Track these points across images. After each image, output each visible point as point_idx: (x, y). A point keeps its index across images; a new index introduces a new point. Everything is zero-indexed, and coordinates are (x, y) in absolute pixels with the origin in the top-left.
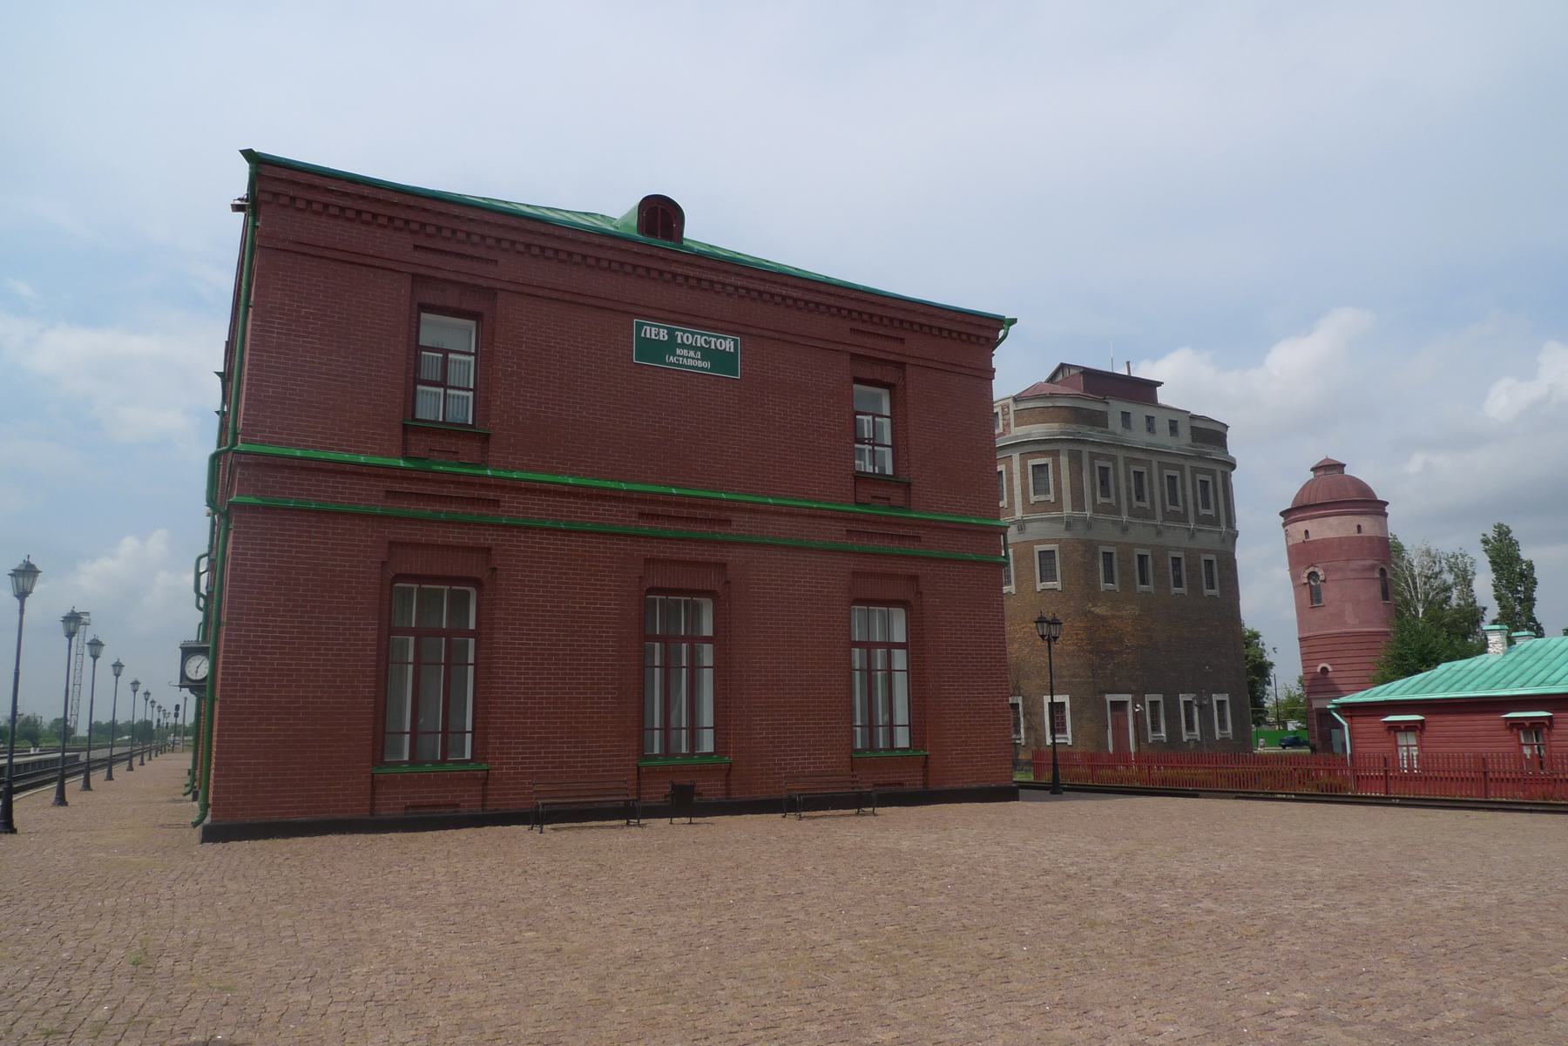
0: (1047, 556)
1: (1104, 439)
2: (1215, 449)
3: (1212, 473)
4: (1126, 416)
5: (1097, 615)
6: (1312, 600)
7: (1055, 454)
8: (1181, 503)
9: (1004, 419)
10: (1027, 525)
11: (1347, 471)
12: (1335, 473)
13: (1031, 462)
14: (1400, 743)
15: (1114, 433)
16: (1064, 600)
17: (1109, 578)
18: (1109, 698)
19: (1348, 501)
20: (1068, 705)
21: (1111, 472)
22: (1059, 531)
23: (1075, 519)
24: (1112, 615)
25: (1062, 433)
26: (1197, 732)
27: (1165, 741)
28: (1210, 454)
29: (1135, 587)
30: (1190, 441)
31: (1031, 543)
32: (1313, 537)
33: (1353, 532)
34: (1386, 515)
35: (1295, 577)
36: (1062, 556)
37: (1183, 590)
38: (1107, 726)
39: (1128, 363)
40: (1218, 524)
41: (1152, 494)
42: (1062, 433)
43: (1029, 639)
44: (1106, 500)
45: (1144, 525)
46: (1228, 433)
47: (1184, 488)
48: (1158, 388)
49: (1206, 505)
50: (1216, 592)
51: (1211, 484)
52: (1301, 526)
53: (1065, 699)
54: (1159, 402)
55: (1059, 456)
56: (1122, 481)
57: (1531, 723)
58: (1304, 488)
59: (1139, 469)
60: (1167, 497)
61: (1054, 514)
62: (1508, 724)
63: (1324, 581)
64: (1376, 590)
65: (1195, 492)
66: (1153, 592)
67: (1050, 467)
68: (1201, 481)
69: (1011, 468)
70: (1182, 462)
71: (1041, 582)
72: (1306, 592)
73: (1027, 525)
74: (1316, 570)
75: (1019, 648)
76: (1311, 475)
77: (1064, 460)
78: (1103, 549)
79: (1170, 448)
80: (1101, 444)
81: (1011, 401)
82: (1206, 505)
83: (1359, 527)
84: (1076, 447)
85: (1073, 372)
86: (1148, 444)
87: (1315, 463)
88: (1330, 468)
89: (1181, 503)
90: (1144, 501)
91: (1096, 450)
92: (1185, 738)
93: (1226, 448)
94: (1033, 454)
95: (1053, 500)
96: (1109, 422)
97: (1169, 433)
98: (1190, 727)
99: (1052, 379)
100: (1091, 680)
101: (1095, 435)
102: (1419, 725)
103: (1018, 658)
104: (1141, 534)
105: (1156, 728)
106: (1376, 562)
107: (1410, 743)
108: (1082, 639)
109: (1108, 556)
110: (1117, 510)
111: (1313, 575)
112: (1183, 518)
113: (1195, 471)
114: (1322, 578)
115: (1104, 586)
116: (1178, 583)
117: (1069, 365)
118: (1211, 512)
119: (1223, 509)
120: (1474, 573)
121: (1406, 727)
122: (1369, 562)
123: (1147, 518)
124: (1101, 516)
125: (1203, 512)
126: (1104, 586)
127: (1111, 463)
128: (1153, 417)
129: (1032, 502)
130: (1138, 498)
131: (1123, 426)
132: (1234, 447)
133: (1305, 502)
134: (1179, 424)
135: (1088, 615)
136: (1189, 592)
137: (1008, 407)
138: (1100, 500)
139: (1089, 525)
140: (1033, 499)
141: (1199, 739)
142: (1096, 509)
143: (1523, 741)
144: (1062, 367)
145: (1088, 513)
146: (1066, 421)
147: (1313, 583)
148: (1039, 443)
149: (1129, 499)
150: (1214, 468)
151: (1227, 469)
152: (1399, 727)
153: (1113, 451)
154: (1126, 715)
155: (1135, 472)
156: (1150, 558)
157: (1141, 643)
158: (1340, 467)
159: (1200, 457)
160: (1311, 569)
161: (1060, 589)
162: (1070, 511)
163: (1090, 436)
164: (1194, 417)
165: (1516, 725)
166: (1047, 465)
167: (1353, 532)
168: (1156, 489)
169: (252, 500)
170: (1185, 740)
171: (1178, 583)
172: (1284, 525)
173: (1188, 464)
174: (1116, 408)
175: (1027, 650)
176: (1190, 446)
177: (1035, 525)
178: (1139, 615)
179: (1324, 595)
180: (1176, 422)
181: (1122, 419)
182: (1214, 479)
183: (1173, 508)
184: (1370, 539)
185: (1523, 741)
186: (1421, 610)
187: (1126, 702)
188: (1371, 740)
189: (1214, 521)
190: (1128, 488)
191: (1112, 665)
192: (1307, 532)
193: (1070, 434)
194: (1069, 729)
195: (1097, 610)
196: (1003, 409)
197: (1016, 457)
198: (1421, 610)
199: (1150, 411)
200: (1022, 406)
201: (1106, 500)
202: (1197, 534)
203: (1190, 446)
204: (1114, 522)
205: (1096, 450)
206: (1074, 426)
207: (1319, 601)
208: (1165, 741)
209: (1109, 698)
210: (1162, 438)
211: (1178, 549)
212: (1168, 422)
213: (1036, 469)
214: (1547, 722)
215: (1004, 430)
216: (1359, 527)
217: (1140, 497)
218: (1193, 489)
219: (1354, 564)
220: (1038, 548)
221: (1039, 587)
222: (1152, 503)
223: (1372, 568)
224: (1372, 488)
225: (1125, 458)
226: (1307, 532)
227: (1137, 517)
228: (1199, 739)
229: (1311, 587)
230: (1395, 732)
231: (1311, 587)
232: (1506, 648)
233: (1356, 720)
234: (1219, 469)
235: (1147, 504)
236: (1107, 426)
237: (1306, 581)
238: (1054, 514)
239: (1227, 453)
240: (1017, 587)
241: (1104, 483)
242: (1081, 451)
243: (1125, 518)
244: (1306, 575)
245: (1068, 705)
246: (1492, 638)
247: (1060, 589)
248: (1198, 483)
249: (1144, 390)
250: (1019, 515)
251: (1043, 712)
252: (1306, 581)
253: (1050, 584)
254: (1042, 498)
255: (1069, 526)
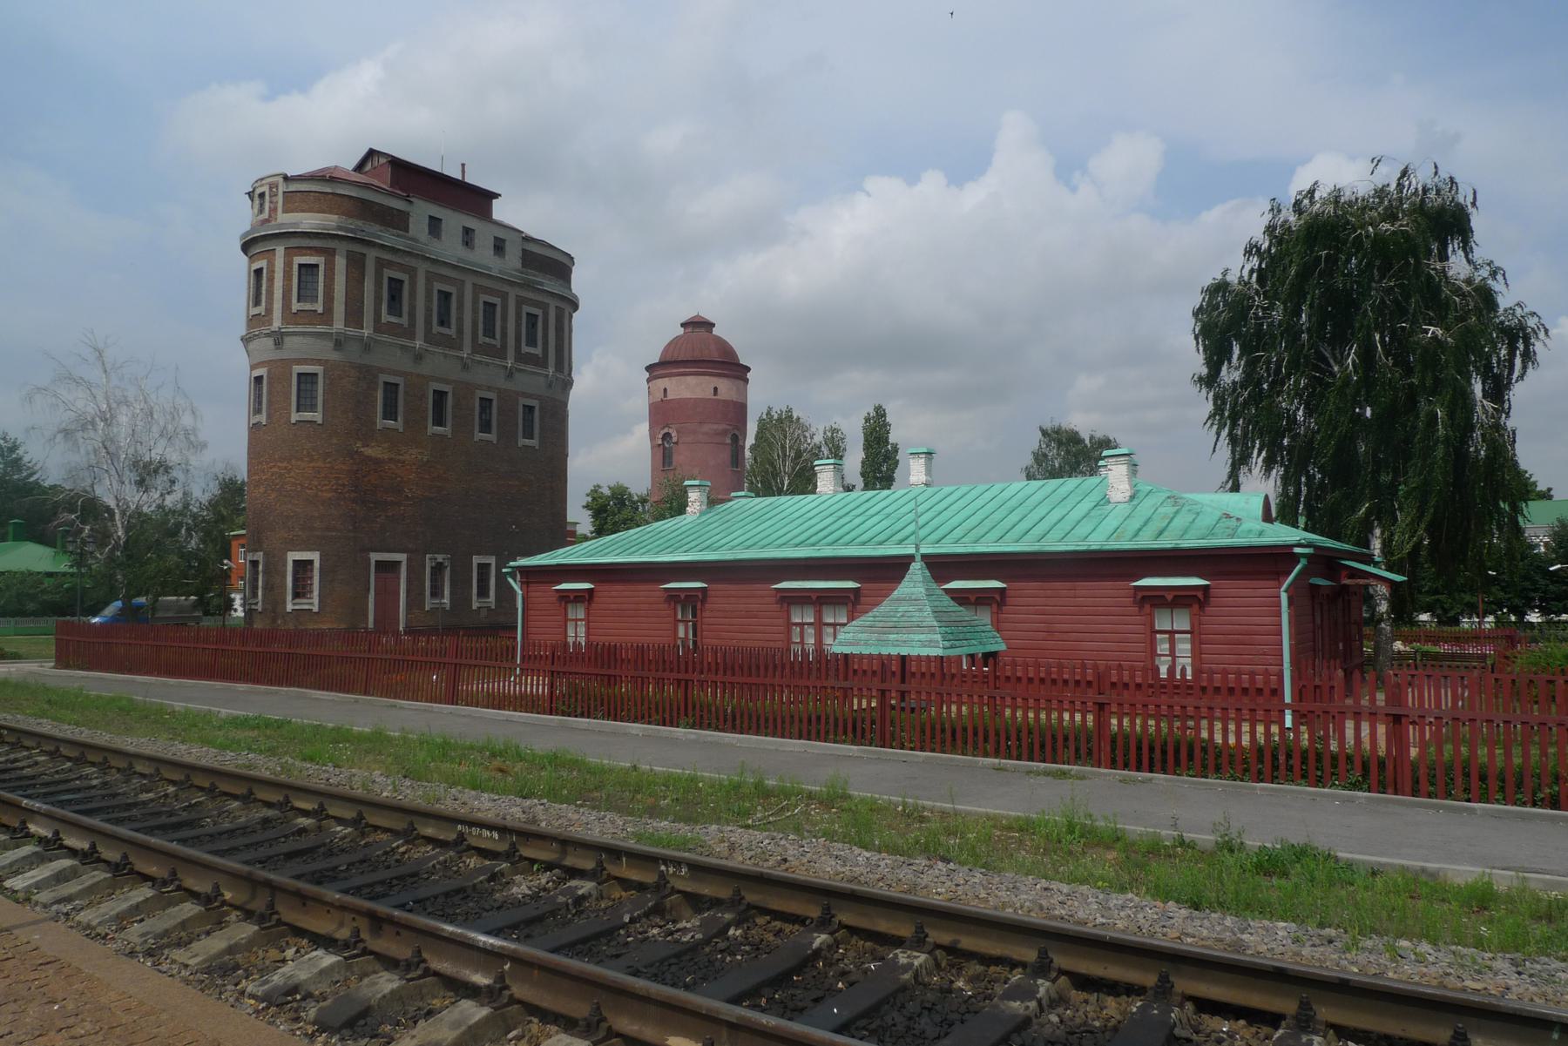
0: (306, 379)
1: (399, 243)
2: (550, 280)
3: (544, 307)
4: (435, 224)
5: (369, 458)
6: (664, 463)
7: (329, 253)
8: (498, 336)
9: (271, 202)
10: (287, 339)
11: (715, 331)
12: (702, 333)
13: (299, 260)
14: (570, 616)
15: (415, 240)
16: (324, 436)
17: (390, 413)
18: (375, 557)
19: (709, 361)
20: (317, 564)
21: (406, 287)
22: (326, 351)
23: (348, 338)
24: (390, 459)
25: (340, 228)
26: (446, 600)
27: (448, 608)
28: (542, 284)
29: (426, 428)
30: (518, 265)
31: (287, 363)
32: (670, 397)
33: (709, 394)
34: (747, 381)
35: (652, 437)
36: (327, 382)
37: (492, 437)
38: (369, 589)
39: (463, 165)
40: (544, 365)
41: (460, 320)
42: (340, 228)
43: (277, 481)
44: (393, 319)
45: (446, 356)
46: (574, 268)
47: (504, 319)
48: (494, 201)
49: (532, 342)
50: (534, 442)
51: (499, 309)
52: (662, 383)
53: (315, 556)
54: (494, 217)
55: (334, 255)
56: (420, 300)
57: (1175, 596)
58: (669, 344)
59: (446, 288)
60: (481, 326)
61: (320, 329)
62: (1139, 597)
63: (676, 443)
64: (725, 455)
65: (518, 325)
66: (450, 436)
67: (322, 268)
68: (528, 314)
69: (273, 265)
70: (506, 288)
71: (298, 411)
72: (660, 452)
73: (287, 339)
74: (671, 431)
75: (265, 492)
76: (681, 331)
77: (340, 263)
78: (383, 378)
79: (489, 269)
80: (393, 250)
81: (281, 180)
82: (532, 342)
83: (716, 389)
84: (357, 248)
85: (383, 160)
86: (460, 260)
87: (684, 319)
88: (699, 325)
89: (498, 336)
90: (449, 328)
91: (387, 256)
92: (289, 607)
93: (569, 282)
94: (301, 250)
95: (320, 310)
96: (411, 226)
97: (492, 253)
98: (483, 592)
99: (359, 167)
100: (351, 534)
101: (388, 238)
102: (1200, 594)
103: (262, 504)
104: (440, 367)
105: (436, 592)
106: (728, 427)
107: (579, 617)
108: (344, 485)
109: (391, 389)
110: (410, 333)
111: (667, 436)
112: (501, 353)
113: (520, 301)
114: (675, 440)
115: (381, 423)
116: (485, 427)
117: (379, 152)
118: (538, 351)
119: (554, 347)
120: (845, 449)
121: (576, 597)
122: (721, 427)
123: (451, 348)
124: (384, 338)
125: (525, 349)
126: (381, 423)
127: (407, 276)
128: (473, 230)
129: (294, 311)
130: (442, 323)
131: (430, 233)
132: (580, 282)
133: (668, 359)
134: (507, 243)
135: (355, 456)
136: (498, 440)
137: (277, 187)
138: (386, 317)
139: (367, 346)
140: (295, 306)
141: (493, 607)
142: (378, 326)
143: (680, 617)
144: (372, 153)
145: (367, 332)
146: (349, 215)
147: (667, 445)
148: (310, 237)
149: (428, 322)
150: (546, 301)
151: (568, 309)
152: (968, 598)
153: (413, 262)
154: (399, 578)
155: (439, 291)
156: (450, 396)
157: (426, 494)
158: (709, 325)
159: (527, 285)
160: (666, 430)
161: (320, 422)
162: (342, 327)
163: (379, 237)
164: (528, 239)
165: (674, 597)
166: (316, 266)
167: (709, 394)
168: (467, 314)
169: (750, 440)
170: (474, 607)
171: (485, 427)
172: (649, 381)
173: (513, 293)
174: (421, 211)
175: (273, 496)
176: (516, 270)
177: (296, 339)
178: (428, 461)
179: (675, 458)
180: (503, 241)
181: (430, 225)
182: (546, 314)
183: (487, 340)
184: (726, 402)
185: (680, 617)
186: (786, 483)
187: (399, 562)
188: (544, 612)
189: (541, 362)
190: (428, 310)
191: (383, 517)
192: (665, 390)
193: (351, 231)
194: (316, 593)
195: (368, 451)
196: (271, 188)
197: (280, 251)
198: (786, 483)
199: (472, 222)
200: (293, 187)
201: (393, 319)
202: (517, 375)
203: (516, 270)
204: (403, 347)
205: (387, 256)
206: (360, 223)
207: (670, 464)
208: (448, 608)
209: (375, 557)
210: (483, 255)
211: (489, 389)
212: (427, 219)
213: (303, 270)
214: (998, 597)
215: (270, 216)
216: (716, 389)
217: (489, 332)
218: (516, 321)
219: (706, 428)
220: (297, 369)
221: (295, 417)
222: (460, 331)
223: (725, 432)
224: (734, 346)
225: (427, 272)
226: (665, 390)
227: (438, 344)
228: (493, 607)
229: (664, 448)
230: (789, 604)
231: (664, 448)
232: (704, 507)
233: (533, 587)
234: (553, 304)
235: (452, 332)
236: (406, 229)
237: (660, 442)
238: (320, 329)
239: (571, 290)
240: (269, 416)
241: (395, 298)
242: (365, 255)
243: (419, 343)
244: (660, 436)
245: (317, 564)
246: (693, 496)
247: (320, 422)
248: (481, 306)
249: (477, 200)
250: (277, 323)
251: (286, 571)
252: (660, 442)
253: (308, 416)
254: (307, 306)
255: (339, 344)
